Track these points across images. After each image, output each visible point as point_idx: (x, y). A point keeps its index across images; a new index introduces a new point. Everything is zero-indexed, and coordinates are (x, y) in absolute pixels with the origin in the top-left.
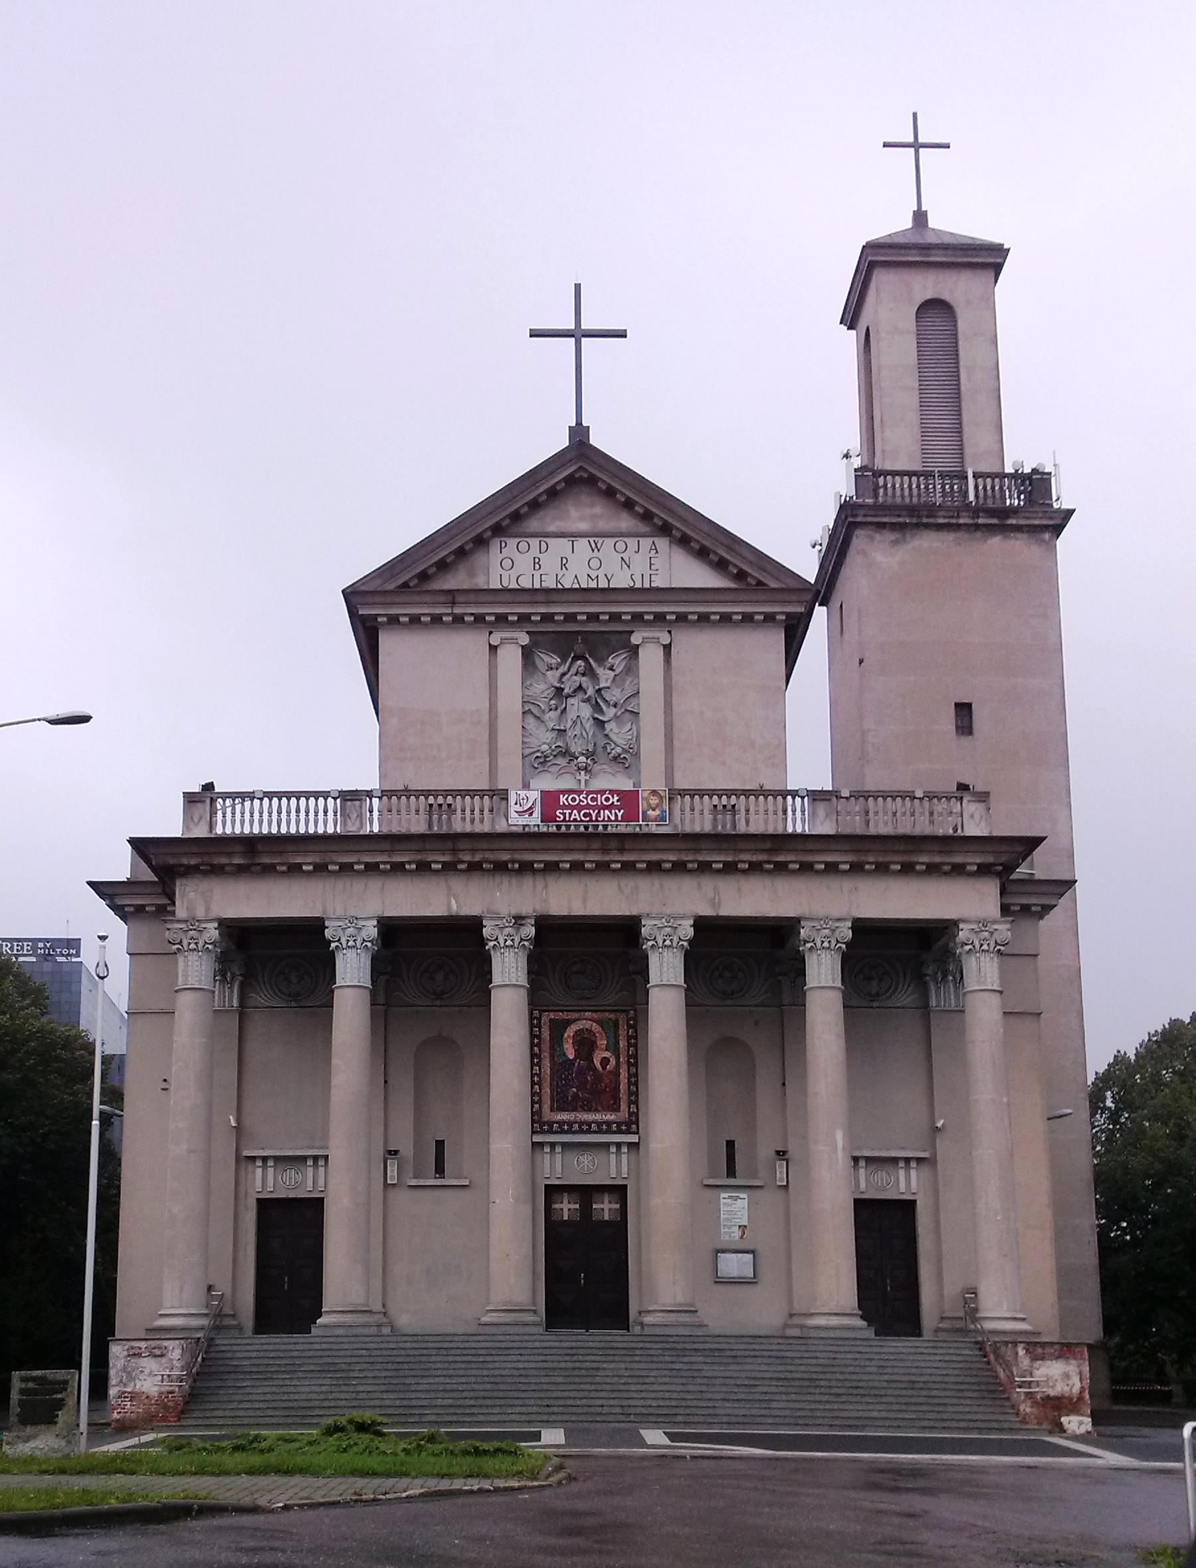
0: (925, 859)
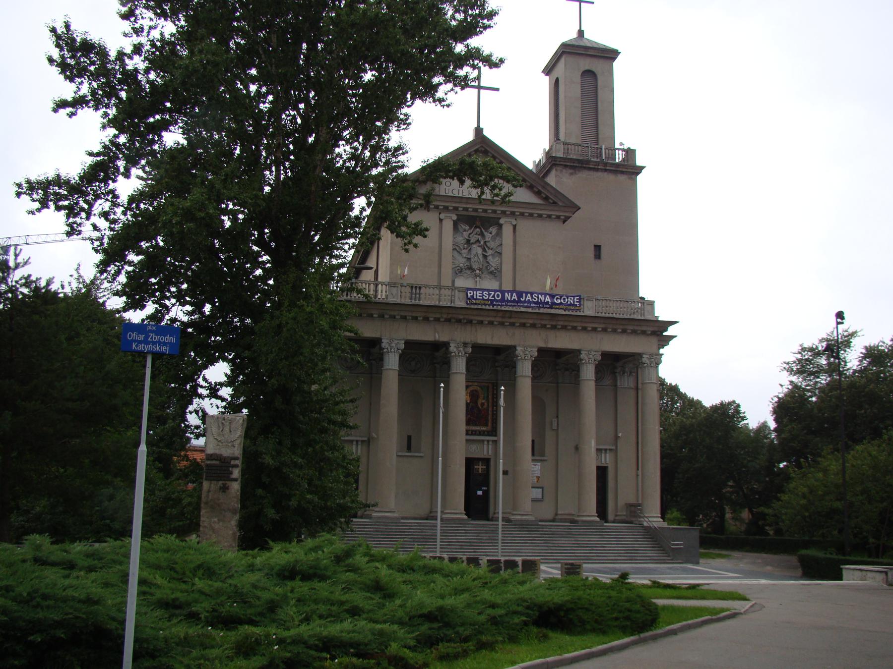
0: (631, 328)
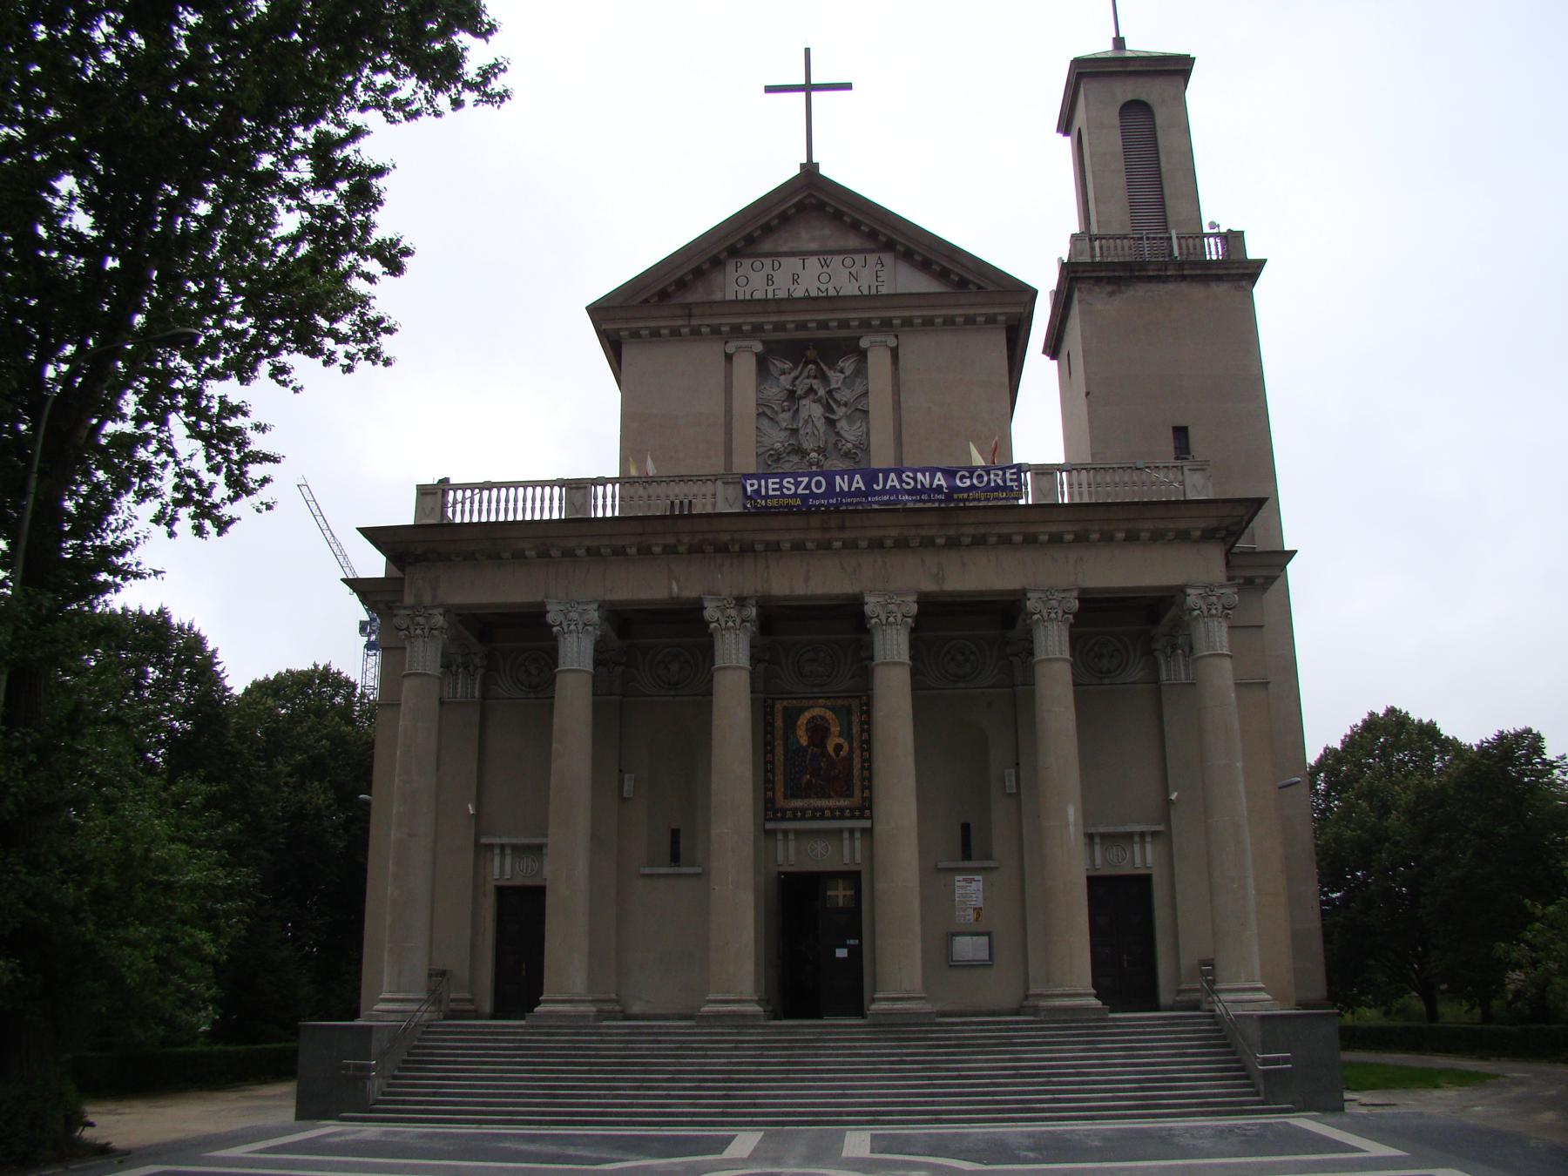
0: (1149, 525)
